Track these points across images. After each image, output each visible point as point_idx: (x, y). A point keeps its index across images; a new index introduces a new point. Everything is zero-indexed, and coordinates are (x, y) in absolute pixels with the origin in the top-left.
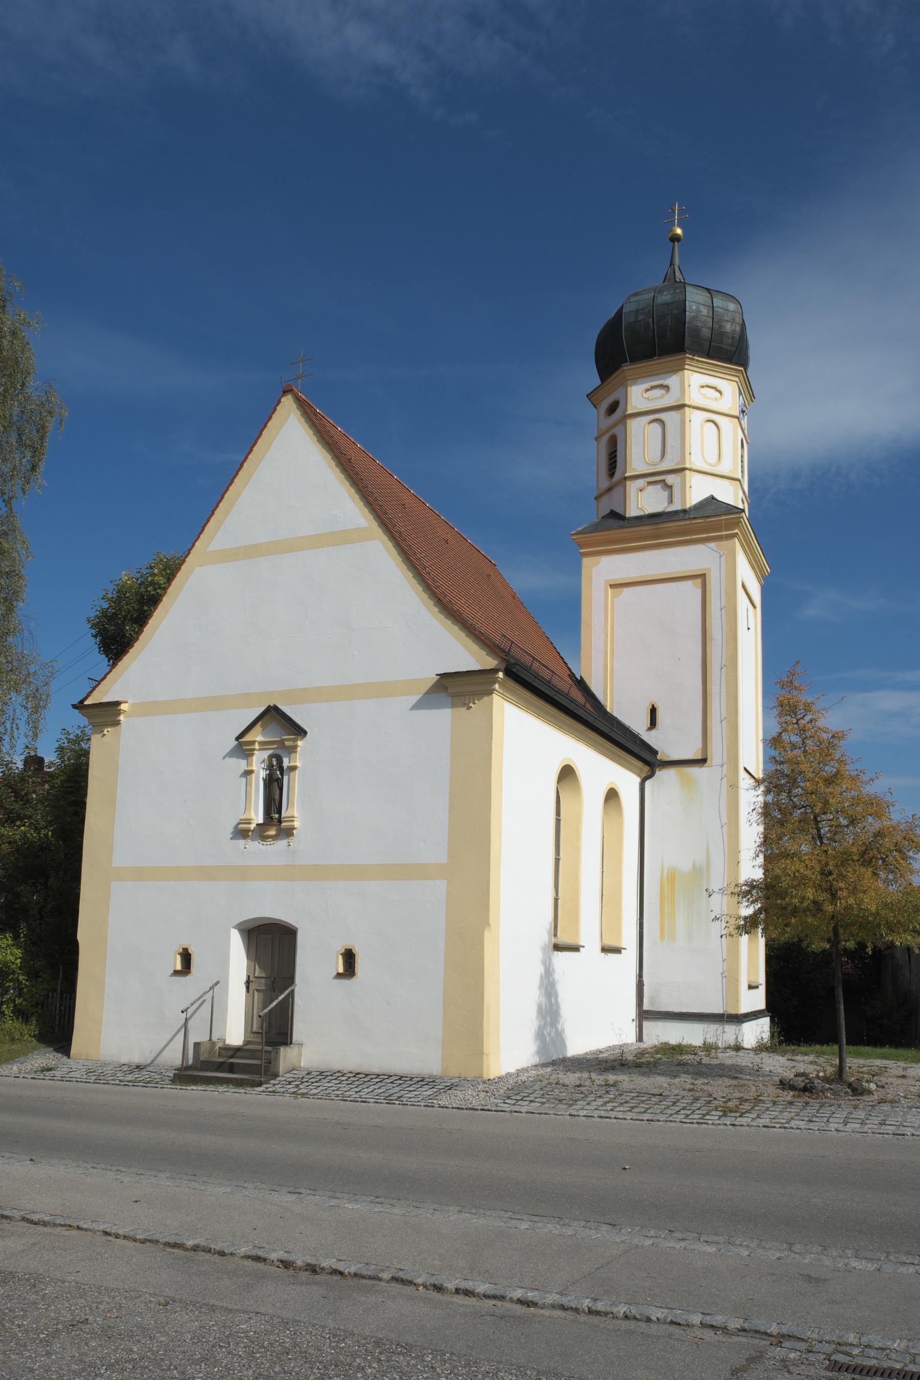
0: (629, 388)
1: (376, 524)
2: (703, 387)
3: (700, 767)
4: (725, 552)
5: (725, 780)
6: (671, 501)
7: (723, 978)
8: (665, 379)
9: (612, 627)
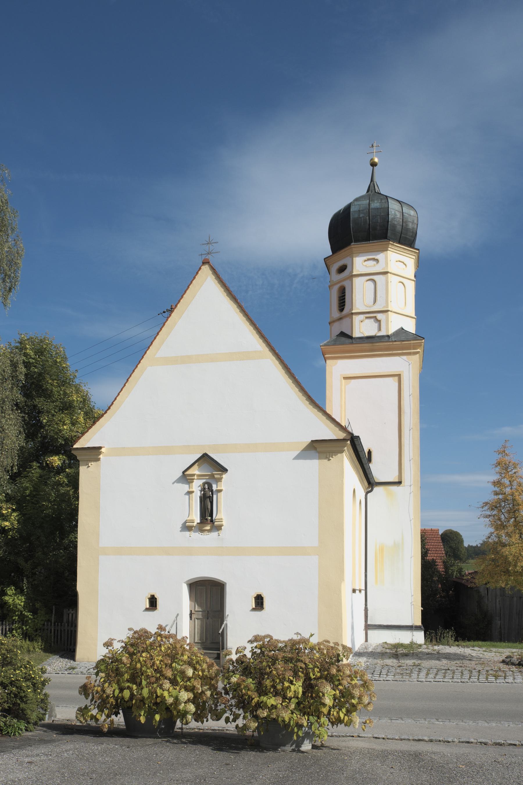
0: (354, 259)
1: (268, 350)
2: (397, 261)
3: (398, 486)
4: (412, 362)
5: (412, 494)
6: (380, 329)
7: (411, 605)
8: (376, 255)
9: (345, 403)
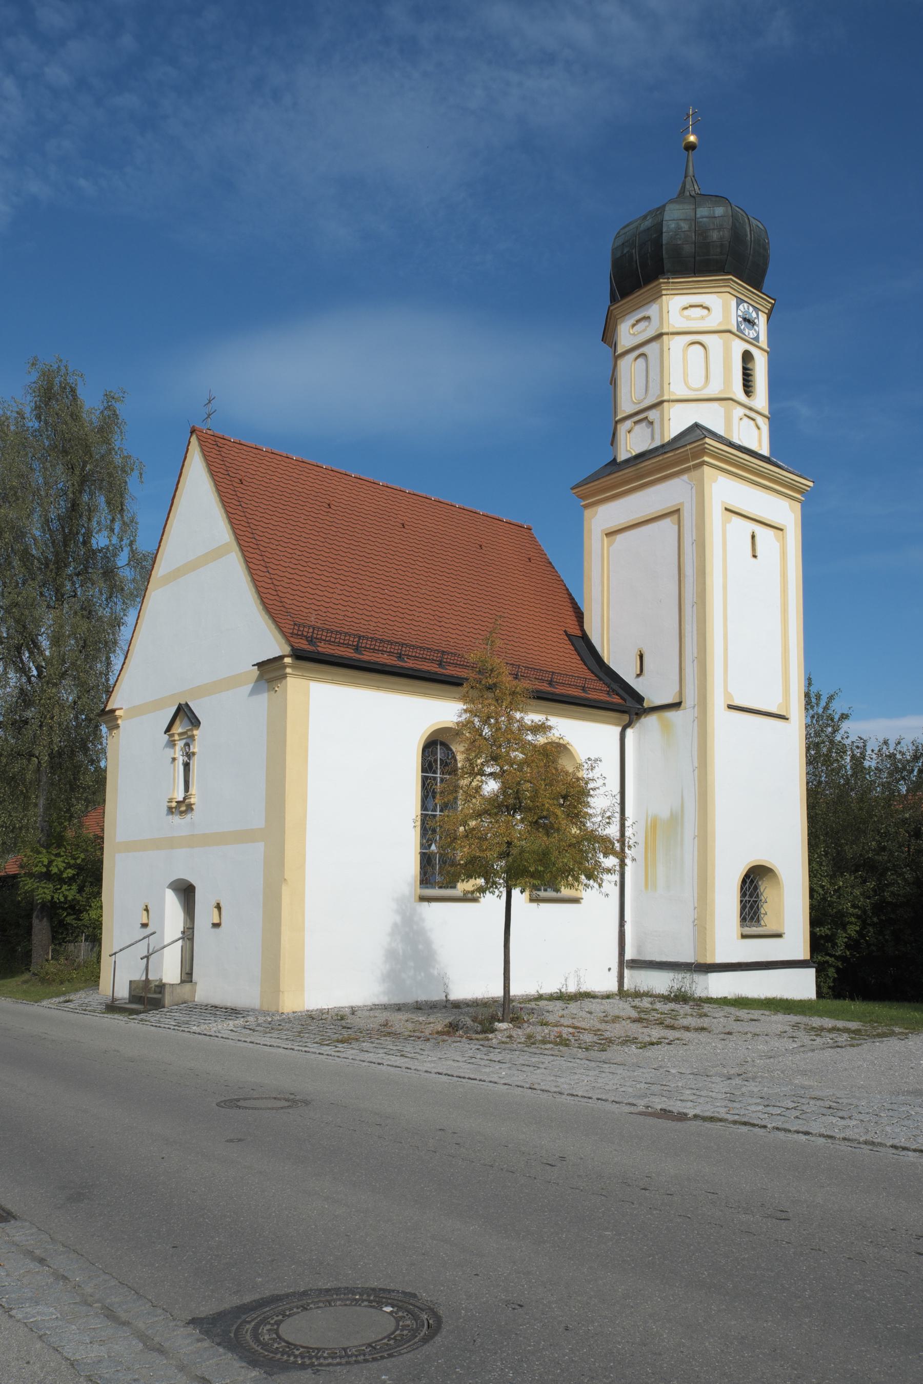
2: (686, 308)
5: (696, 722)
6: (653, 438)
